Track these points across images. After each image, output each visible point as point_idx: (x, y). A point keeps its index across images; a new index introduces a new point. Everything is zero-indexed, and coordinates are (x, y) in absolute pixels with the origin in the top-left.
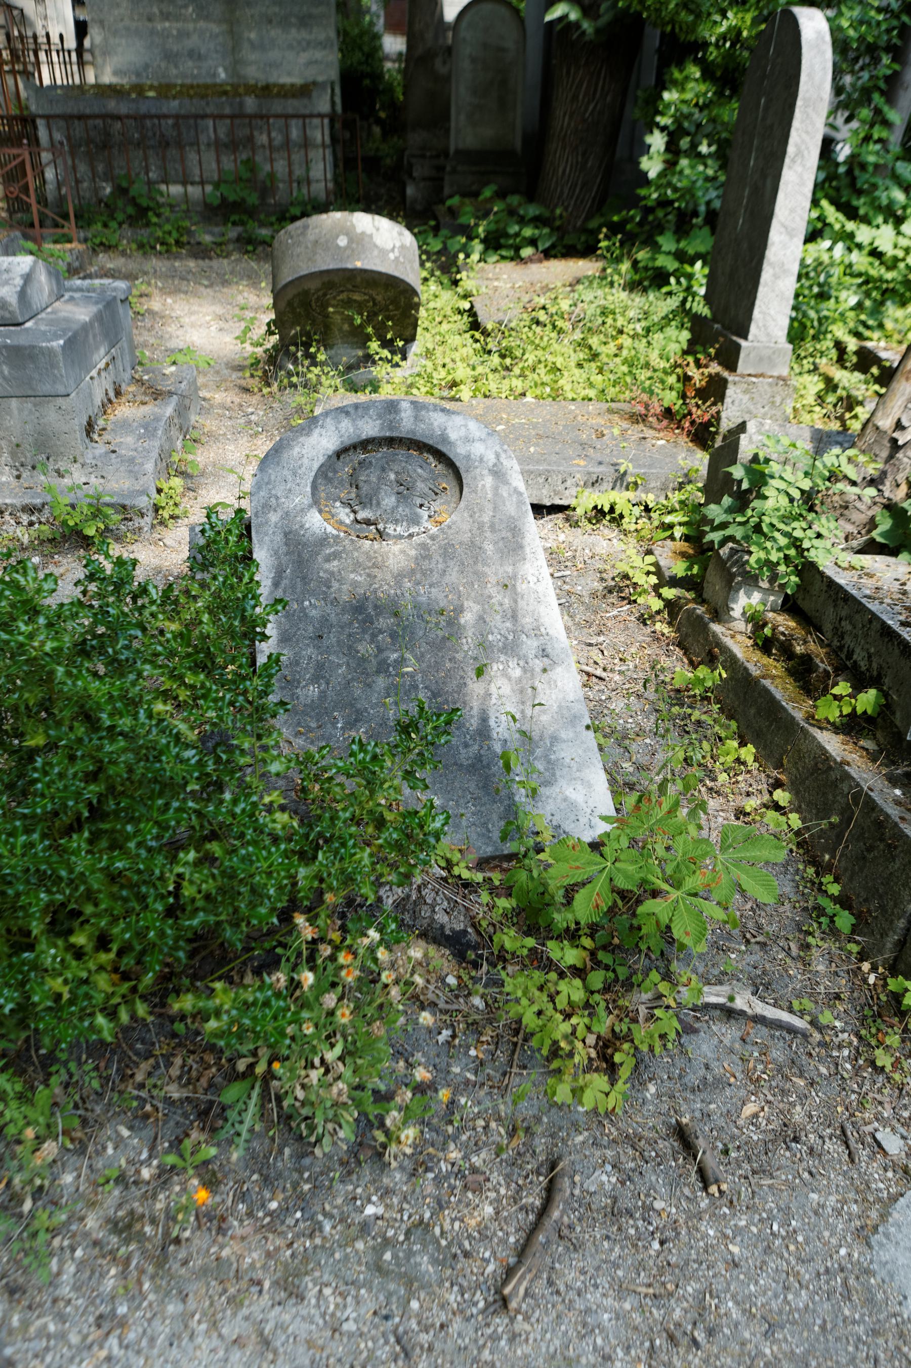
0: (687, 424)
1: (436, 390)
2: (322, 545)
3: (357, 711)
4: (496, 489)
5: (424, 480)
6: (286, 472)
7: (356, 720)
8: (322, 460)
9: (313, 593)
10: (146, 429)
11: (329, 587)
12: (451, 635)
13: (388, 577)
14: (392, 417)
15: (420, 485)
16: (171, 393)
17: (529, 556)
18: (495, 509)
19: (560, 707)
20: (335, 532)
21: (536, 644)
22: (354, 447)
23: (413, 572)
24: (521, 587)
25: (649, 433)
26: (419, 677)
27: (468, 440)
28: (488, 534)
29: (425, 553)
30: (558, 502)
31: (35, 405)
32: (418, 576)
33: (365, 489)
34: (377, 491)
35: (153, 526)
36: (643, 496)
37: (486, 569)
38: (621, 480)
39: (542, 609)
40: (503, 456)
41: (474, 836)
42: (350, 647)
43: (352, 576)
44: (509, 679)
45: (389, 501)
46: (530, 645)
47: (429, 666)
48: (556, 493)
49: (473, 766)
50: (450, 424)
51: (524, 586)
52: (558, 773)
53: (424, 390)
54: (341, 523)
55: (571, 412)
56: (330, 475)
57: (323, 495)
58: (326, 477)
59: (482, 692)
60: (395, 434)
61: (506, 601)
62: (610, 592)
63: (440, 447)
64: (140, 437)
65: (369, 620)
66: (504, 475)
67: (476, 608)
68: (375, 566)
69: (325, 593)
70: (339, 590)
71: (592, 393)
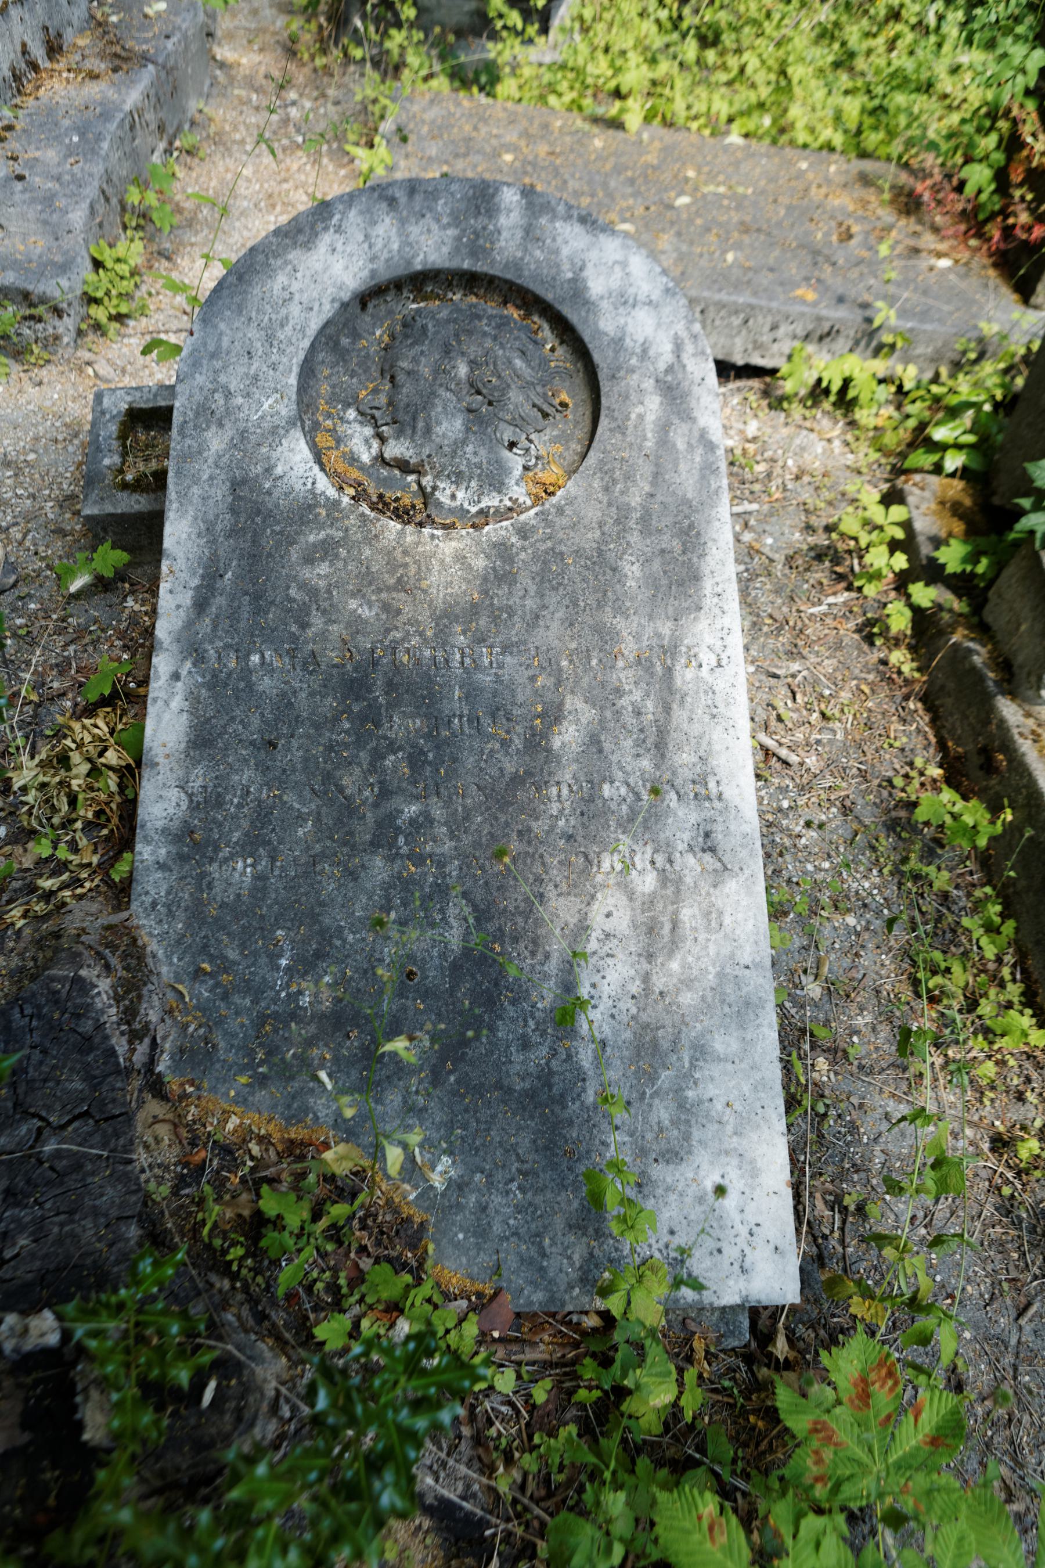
0: (996, 235)
1: (587, 102)
2: (303, 522)
3: (322, 932)
4: (664, 428)
5: (527, 386)
6: (252, 333)
7: (319, 955)
8: (328, 310)
9: (270, 635)
10: (82, 135)
11: (304, 626)
12: (529, 773)
13: (424, 616)
14: (482, 220)
15: (515, 397)
16: (145, 59)
17: (709, 602)
18: (657, 476)
19: (721, 975)
20: (332, 492)
21: (693, 818)
23: (474, 609)
24: (684, 676)
25: (929, 241)
26: (453, 868)
27: (625, 301)
28: (634, 538)
29: (502, 570)
30: (757, 361)
32: (483, 622)
33: (407, 389)
34: (428, 398)
35: (80, 333)
36: (899, 369)
37: (619, 623)
38: (871, 340)
39: (717, 734)
40: (689, 348)
41: (511, 1262)
42: (328, 777)
43: (353, 604)
44: (631, 896)
45: (450, 427)
46: (682, 819)
47: (477, 844)
48: (758, 346)
49: (531, 1094)
51: (689, 674)
52: (696, 1134)
53: (568, 97)
54: (353, 459)
55: (801, 174)
56: (345, 341)
57: (325, 388)
58: (334, 346)
59: (573, 921)
60: (481, 267)
61: (650, 705)
62: (819, 558)
64: (70, 151)
65: (372, 717)
66: (685, 395)
67: (588, 714)
68: (401, 585)
69: (294, 638)
70: (324, 634)
71: (838, 139)
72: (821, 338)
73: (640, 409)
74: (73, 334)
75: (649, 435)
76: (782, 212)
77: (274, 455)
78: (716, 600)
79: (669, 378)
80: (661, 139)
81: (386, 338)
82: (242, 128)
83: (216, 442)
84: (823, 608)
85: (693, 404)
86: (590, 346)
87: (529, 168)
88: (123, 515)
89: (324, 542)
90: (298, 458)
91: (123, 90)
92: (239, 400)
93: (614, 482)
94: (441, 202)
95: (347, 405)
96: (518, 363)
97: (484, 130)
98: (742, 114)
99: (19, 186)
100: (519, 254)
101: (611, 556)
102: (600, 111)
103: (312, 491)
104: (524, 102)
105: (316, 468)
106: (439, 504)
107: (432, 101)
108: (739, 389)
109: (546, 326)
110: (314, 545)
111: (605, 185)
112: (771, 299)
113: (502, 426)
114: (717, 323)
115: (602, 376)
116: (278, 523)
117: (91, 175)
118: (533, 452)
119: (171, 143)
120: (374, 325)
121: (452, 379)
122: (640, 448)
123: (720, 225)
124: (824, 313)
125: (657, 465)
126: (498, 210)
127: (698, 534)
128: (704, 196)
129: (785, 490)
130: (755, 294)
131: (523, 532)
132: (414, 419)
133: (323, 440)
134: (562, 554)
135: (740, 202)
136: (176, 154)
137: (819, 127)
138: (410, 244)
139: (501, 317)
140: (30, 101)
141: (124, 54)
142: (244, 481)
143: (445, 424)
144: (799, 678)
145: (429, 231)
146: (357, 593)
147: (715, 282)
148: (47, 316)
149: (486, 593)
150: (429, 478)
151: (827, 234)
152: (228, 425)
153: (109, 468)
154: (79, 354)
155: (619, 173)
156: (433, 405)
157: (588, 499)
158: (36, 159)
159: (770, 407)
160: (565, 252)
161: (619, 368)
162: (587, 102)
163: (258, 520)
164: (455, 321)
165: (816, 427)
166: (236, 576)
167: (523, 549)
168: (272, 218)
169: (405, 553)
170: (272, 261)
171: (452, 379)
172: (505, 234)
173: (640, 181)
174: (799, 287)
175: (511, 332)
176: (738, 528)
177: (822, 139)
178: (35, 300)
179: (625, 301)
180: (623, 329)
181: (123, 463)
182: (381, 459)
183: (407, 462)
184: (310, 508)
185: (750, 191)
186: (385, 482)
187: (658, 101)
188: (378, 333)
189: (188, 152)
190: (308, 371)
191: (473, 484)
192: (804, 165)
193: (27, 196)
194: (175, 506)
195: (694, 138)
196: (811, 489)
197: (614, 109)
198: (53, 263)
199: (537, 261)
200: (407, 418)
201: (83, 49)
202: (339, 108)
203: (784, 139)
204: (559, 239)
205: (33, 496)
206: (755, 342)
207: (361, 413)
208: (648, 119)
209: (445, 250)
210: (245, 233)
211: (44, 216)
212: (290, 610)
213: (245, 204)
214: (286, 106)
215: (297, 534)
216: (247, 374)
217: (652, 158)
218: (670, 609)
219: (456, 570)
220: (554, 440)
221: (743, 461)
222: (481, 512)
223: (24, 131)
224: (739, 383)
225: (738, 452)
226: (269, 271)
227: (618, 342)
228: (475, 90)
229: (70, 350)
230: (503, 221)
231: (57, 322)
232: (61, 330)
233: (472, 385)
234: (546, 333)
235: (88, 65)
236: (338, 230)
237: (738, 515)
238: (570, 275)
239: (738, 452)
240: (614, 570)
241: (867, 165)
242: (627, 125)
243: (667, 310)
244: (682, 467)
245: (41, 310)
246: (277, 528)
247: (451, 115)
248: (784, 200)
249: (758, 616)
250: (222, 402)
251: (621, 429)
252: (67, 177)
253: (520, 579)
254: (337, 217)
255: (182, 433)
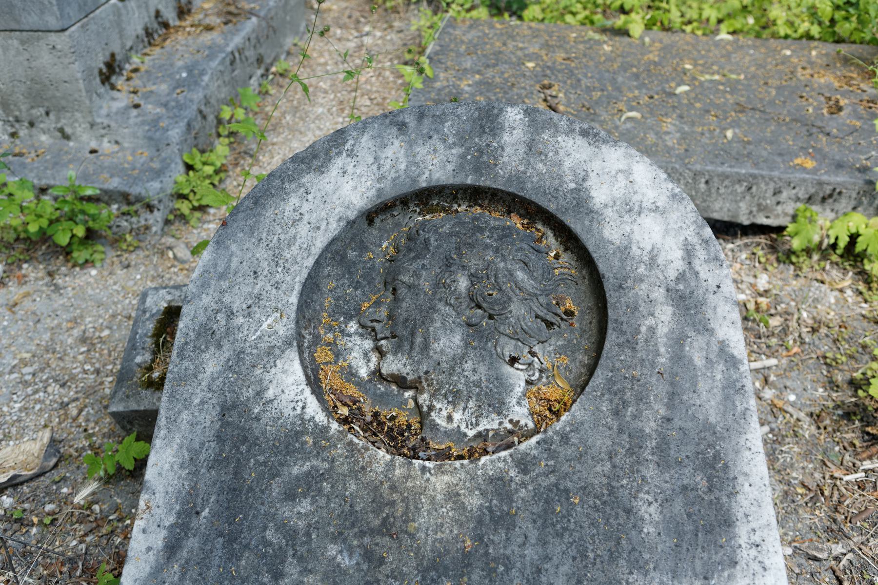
1: (598, 17)
2: (289, 451)
4: (678, 341)
8: (334, 228)
15: (517, 309)
17: (745, 554)
22: (404, 201)
27: (629, 208)
28: (650, 472)
30: (762, 220)
31: (23, 43)
35: (167, 222)
40: (701, 254)
43: (332, 550)
45: (448, 342)
48: (761, 208)
50: (596, 165)
54: (350, 374)
56: (352, 254)
60: (485, 182)
62: (848, 416)
63: (570, 221)
68: (386, 528)
72: (824, 200)
73: (650, 321)
74: (160, 224)
75: (662, 350)
76: (774, 92)
77: (267, 377)
78: (753, 552)
79: (681, 287)
80: (661, 41)
81: (391, 250)
82: (326, 54)
83: (212, 364)
84: (860, 475)
85: (709, 314)
86: (594, 255)
87: (548, 72)
88: (145, 411)
89: (308, 474)
90: (290, 380)
91: (229, 36)
92: (240, 320)
93: (625, 404)
94: (447, 124)
95: (349, 318)
96: (520, 275)
97: (511, 45)
98: (729, 16)
99: (135, 112)
100: (522, 168)
101: (623, 494)
102: (609, 23)
103: (301, 417)
104: (546, 22)
105: (308, 391)
106: (435, 427)
107: (471, 27)
108: (746, 245)
109: (550, 233)
110: (298, 478)
111: (613, 81)
112: (771, 169)
113: (503, 340)
114: (722, 191)
115: (608, 286)
116: (263, 452)
117: (191, 101)
118: (537, 366)
119: (267, 70)
120: (381, 238)
121: (452, 293)
122: (653, 364)
123: (718, 107)
124: (825, 178)
125: (672, 384)
126: (502, 129)
127: (726, 467)
128: (701, 84)
129: (803, 343)
130: (756, 165)
131: (524, 464)
132: (413, 334)
133: (322, 355)
134: (567, 491)
135: (734, 87)
136: (271, 77)
137: (797, 21)
138: (416, 164)
139: (504, 228)
140: (157, 50)
141: (236, 11)
142: (234, 406)
143: (443, 341)
144: (844, 562)
145: (435, 151)
146: (338, 537)
147: (716, 156)
148: (141, 211)
149: (480, 538)
150: (426, 396)
151: (818, 108)
152: (226, 345)
153: (139, 365)
154: (163, 240)
155: (625, 71)
156: (432, 320)
157: (596, 426)
158: (151, 92)
159: (778, 260)
160: (568, 163)
161: (626, 278)
162: (598, 17)
163: (243, 448)
164: (457, 234)
165: (826, 277)
166: (214, 514)
167: (523, 484)
168: (341, 120)
169: (393, 488)
170: (287, 185)
171: (452, 293)
172: (508, 150)
173: (644, 75)
174: (797, 156)
175: (513, 245)
176: (757, 384)
177: (801, 31)
178: (132, 198)
179: (629, 208)
180: (628, 237)
181: (153, 361)
182: (377, 374)
183: (404, 378)
184: (298, 434)
185: (742, 77)
186: (381, 399)
187: (657, 12)
188: (384, 245)
189: (281, 75)
190: (311, 286)
191: (471, 404)
192: (788, 53)
193: (140, 119)
194: (163, 432)
195: (688, 38)
196: (829, 342)
197: (620, 21)
198: (151, 170)
199: (540, 174)
200: (406, 333)
201: (206, 10)
202: (401, 35)
203: (766, 34)
204: (562, 152)
205: (97, 372)
206: (759, 205)
207: (363, 326)
208: (648, 26)
209: (450, 167)
210: (318, 133)
211: (150, 134)
212: (264, 556)
213: (320, 110)
214: (362, 36)
215: (282, 465)
216: (250, 294)
217: (653, 57)
218: (698, 564)
219: (447, 510)
220: (558, 351)
221: (757, 317)
222: (479, 435)
223: (147, 72)
224: (746, 240)
225: (751, 306)
226: (283, 194)
227: (624, 251)
228: (506, 15)
229: (157, 238)
230: (506, 138)
231: (148, 215)
232: (151, 222)
233: (472, 299)
234: (551, 240)
235: (207, 21)
236: (351, 154)
237: (757, 371)
238: (573, 186)
239: (751, 306)
240: (628, 511)
241: (844, 49)
242: (631, 33)
243: (674, 216)
244: (702, 386)
245: (137, 206)
246: (261, 458)
247: (486, 35)
248: (773, 82)
249: (789, 484)
250: (223, 322)
251: (631, 344)
252: (173, 104)
253: (519, 522)
254: (351, 142)
255: (181, 356)
